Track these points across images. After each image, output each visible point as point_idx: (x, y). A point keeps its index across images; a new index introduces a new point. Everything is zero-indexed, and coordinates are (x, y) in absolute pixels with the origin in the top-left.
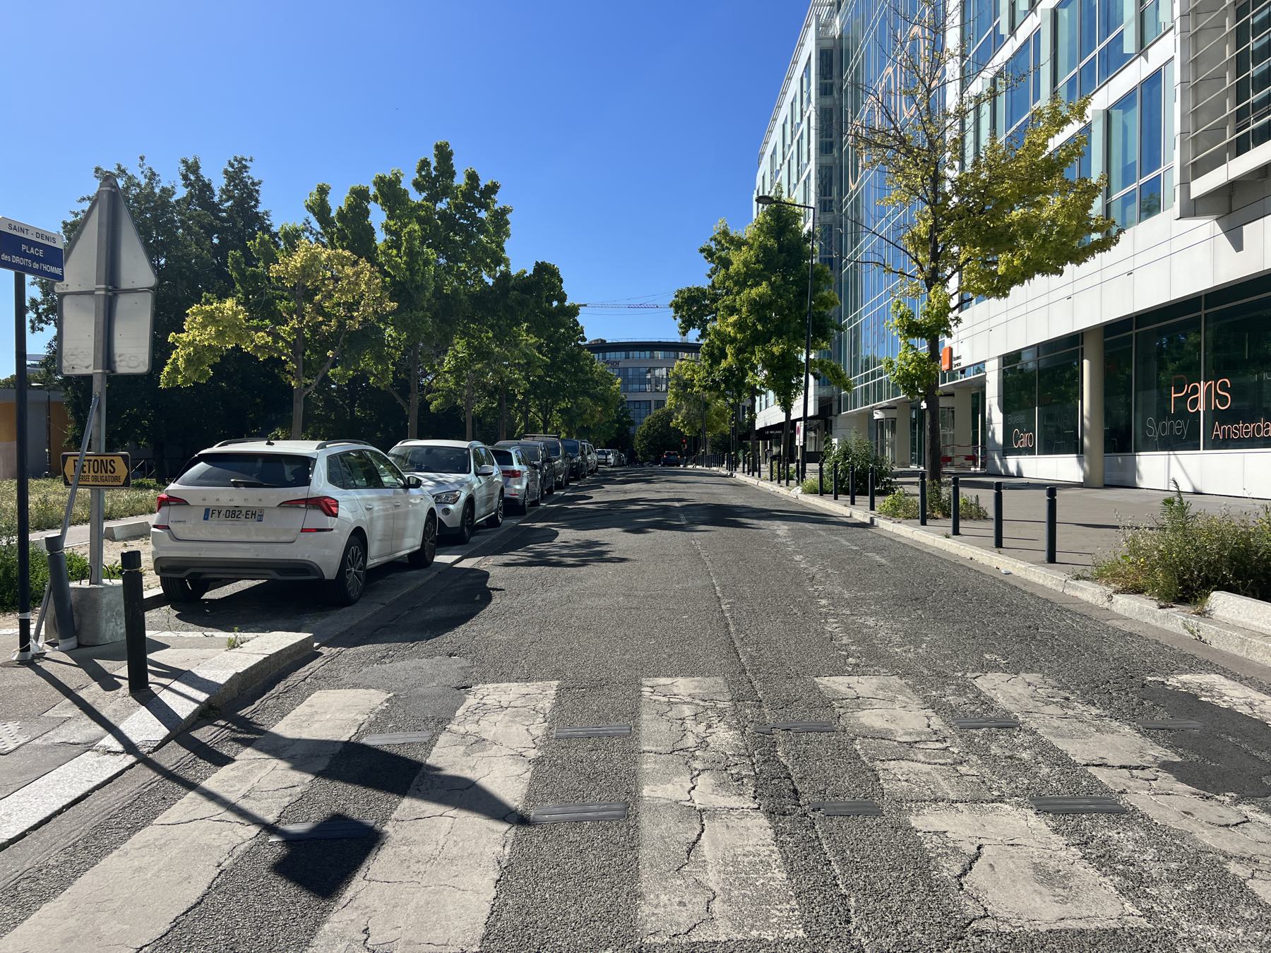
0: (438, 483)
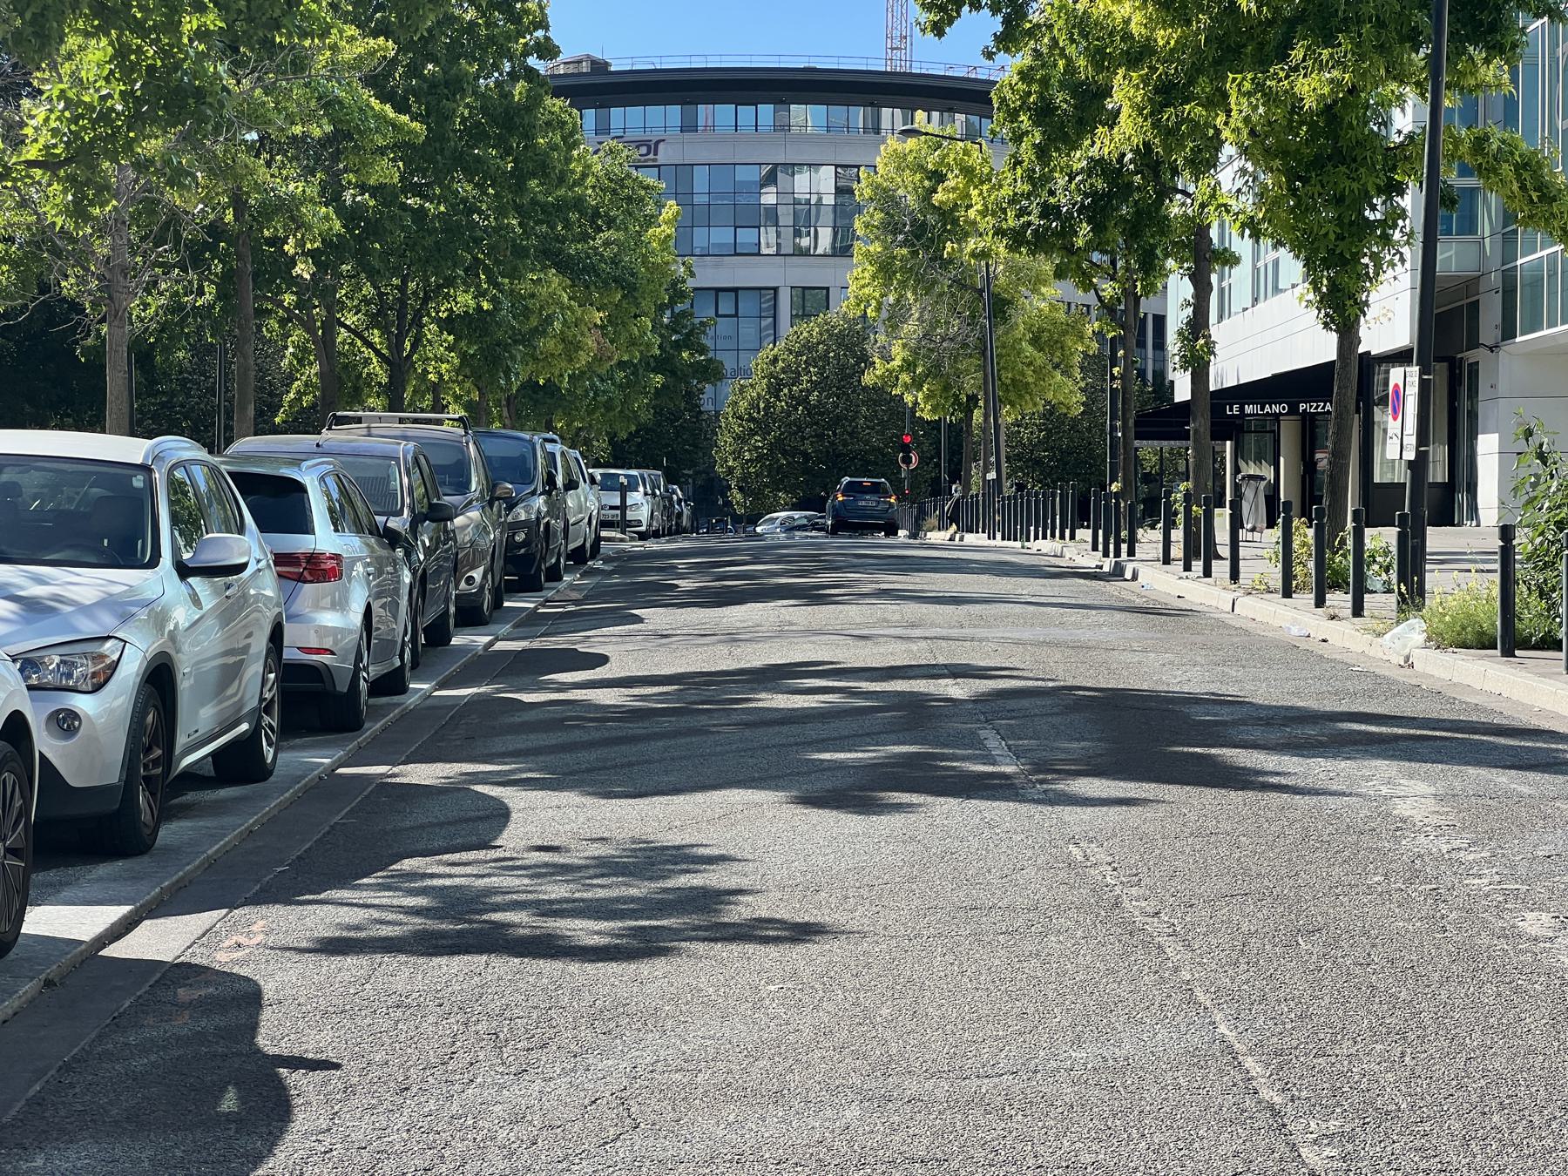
0: (33, 608)
